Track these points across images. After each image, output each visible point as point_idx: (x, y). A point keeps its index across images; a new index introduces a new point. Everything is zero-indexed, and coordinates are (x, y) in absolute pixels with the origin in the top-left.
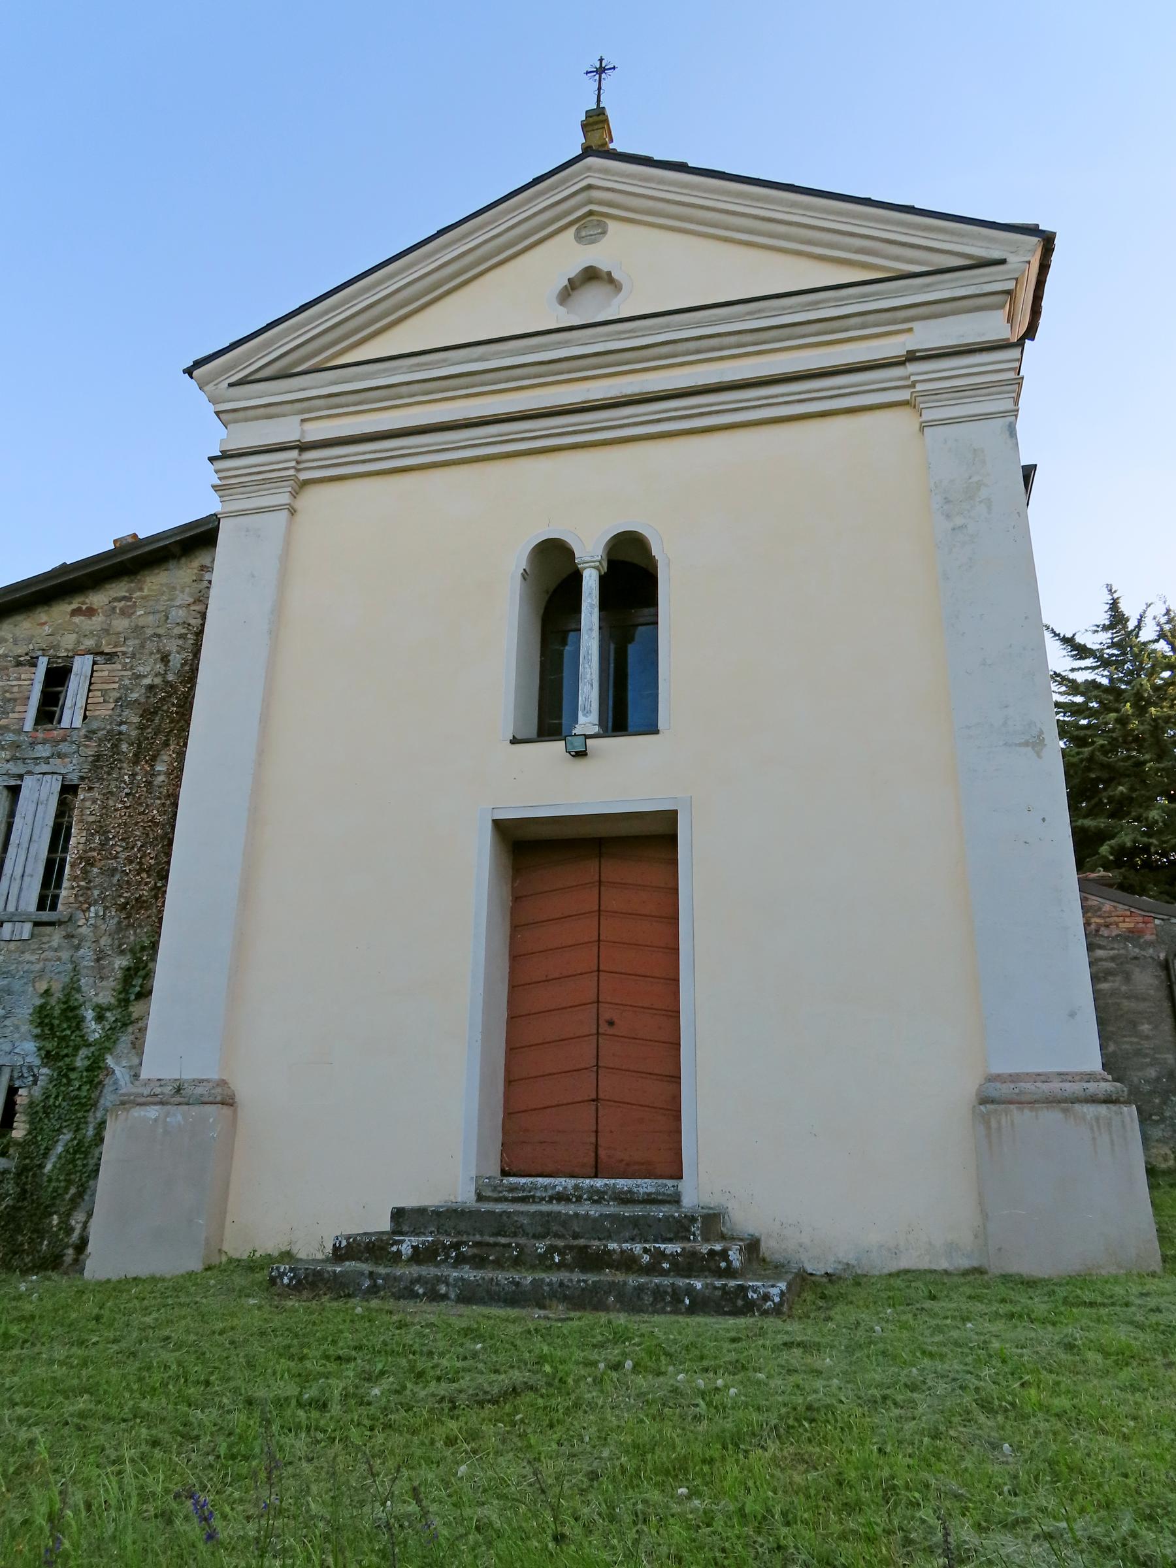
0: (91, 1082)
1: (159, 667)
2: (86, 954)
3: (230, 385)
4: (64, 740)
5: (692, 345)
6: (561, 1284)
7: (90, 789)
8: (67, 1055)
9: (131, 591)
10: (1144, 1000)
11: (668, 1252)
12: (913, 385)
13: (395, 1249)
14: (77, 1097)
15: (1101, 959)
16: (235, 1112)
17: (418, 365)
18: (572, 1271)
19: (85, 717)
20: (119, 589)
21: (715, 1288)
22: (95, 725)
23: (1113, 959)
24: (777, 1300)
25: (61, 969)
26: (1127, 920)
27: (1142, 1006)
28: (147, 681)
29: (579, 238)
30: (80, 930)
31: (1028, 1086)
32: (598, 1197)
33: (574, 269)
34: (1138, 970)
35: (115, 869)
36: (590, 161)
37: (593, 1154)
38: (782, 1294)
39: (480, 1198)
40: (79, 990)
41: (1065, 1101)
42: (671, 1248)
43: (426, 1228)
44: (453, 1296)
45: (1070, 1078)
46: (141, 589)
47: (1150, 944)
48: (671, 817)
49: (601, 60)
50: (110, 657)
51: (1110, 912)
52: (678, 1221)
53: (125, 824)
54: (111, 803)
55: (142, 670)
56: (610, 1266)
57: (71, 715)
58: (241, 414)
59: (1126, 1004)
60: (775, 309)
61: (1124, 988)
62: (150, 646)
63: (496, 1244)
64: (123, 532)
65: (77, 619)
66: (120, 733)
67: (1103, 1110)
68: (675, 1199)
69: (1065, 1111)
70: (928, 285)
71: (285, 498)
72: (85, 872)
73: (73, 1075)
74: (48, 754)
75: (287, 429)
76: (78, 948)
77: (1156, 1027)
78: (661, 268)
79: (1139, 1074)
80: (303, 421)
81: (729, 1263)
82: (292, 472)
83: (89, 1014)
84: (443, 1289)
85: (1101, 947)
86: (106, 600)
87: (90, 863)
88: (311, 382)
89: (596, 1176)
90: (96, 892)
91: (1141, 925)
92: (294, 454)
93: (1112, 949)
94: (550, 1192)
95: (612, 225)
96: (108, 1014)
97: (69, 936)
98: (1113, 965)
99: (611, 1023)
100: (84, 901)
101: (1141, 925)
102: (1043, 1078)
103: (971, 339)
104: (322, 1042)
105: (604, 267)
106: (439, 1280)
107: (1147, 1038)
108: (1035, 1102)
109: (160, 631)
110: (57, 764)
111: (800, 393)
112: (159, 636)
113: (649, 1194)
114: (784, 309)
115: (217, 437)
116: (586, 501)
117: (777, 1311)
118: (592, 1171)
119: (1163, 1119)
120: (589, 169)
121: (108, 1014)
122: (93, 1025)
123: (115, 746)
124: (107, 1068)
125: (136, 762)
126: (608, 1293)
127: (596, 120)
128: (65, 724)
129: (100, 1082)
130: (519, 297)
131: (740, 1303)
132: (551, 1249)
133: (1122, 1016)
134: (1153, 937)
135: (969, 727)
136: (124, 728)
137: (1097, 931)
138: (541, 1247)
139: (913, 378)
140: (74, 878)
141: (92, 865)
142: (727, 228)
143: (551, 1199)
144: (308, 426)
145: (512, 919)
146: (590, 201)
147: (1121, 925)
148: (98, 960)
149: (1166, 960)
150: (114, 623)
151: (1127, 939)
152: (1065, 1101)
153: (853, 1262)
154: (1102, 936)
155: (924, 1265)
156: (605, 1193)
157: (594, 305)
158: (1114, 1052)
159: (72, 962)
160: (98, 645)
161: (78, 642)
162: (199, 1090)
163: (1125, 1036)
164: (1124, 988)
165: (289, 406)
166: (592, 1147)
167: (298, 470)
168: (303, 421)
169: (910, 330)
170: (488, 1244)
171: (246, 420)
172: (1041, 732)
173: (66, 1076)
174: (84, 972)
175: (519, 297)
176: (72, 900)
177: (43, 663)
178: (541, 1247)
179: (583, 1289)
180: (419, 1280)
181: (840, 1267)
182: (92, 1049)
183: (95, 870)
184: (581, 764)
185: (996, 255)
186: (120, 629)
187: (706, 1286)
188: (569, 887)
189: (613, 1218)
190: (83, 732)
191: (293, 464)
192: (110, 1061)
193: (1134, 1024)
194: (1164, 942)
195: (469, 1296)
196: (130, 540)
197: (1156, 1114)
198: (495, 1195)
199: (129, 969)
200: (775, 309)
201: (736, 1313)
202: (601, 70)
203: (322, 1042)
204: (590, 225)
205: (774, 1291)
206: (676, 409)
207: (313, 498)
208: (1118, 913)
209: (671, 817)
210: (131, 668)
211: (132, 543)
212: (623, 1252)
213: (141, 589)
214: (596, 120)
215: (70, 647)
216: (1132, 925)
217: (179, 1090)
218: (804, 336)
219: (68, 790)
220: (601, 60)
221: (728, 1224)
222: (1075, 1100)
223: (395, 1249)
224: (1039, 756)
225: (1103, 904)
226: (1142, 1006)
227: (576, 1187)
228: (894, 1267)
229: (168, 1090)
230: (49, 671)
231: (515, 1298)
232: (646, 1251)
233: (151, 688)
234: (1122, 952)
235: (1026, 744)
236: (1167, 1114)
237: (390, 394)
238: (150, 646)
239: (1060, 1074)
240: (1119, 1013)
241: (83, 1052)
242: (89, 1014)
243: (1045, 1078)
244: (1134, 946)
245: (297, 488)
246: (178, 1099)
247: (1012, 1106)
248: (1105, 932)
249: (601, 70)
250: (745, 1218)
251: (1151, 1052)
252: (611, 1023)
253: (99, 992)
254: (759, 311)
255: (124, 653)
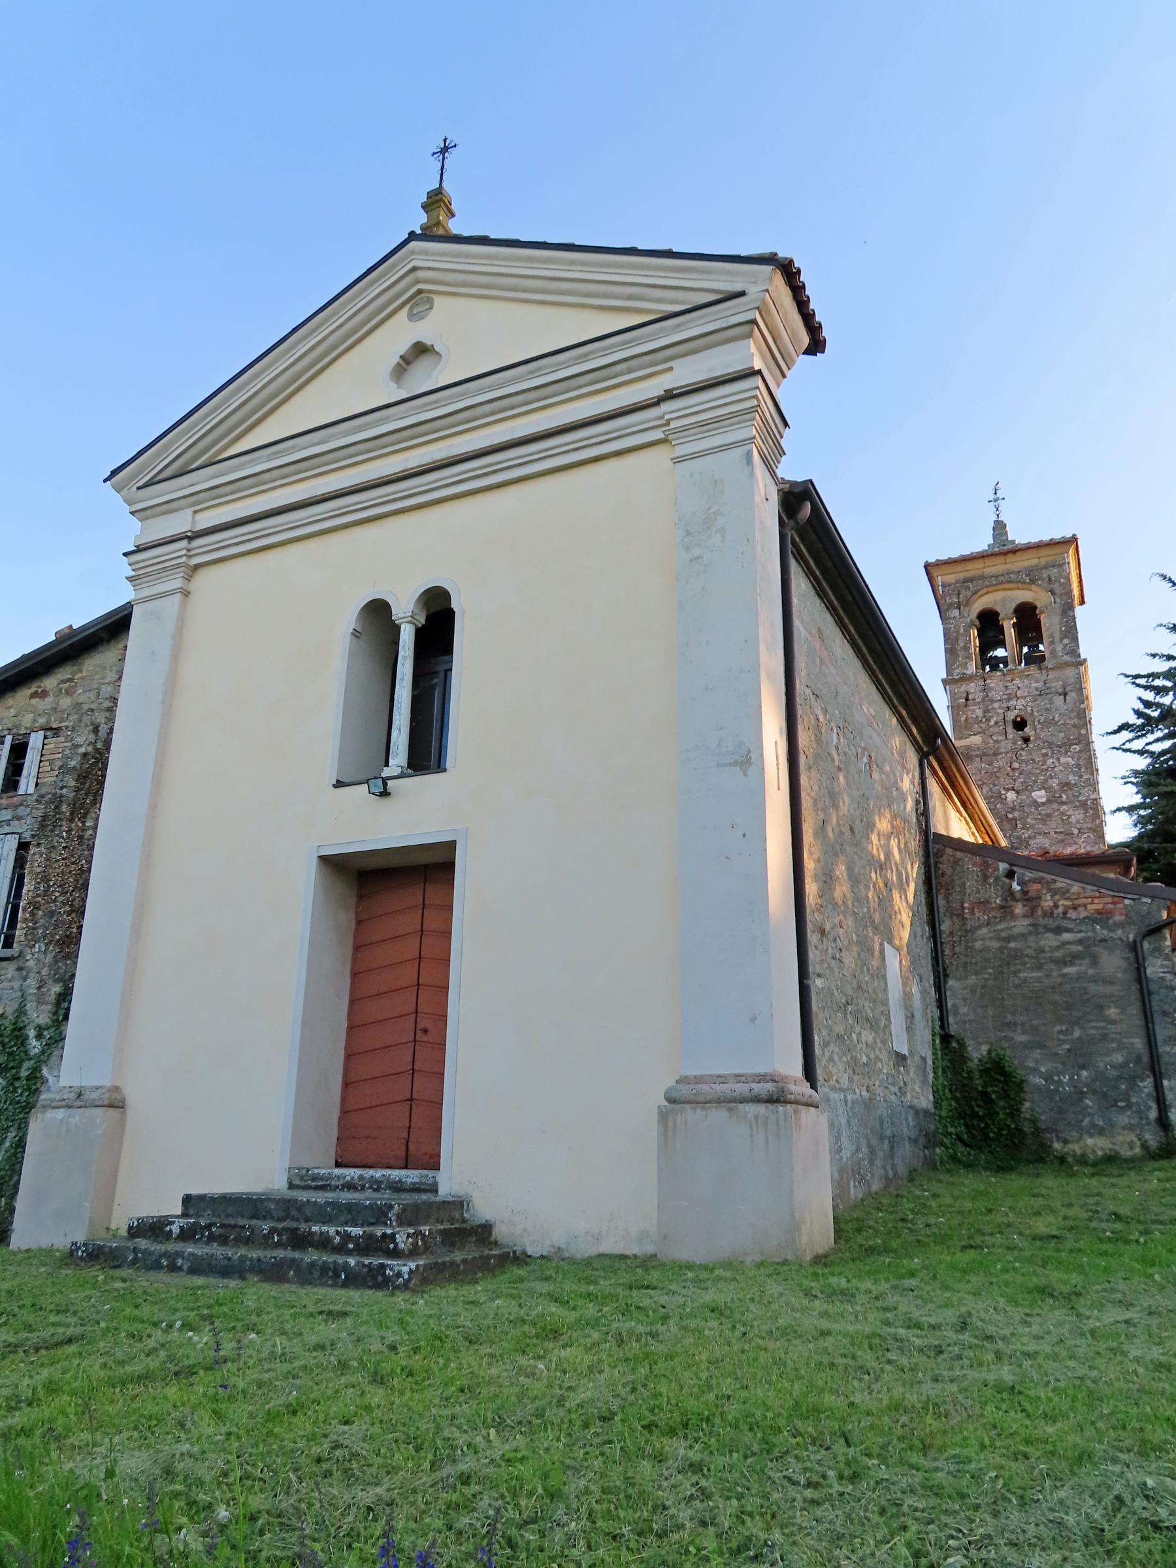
0: (29, 1089)
1: (92, 737)
2: (32, 983)
3: (138, 488)
4: (21, 805)
5: (487, 408)
6: (259, 1260)
7: (39, 845)
8: (13, 1068)
9: (74, 674)
10: (1112, 983)
11: (353, 1234)
12: (668, 423)
13: (168, 1228)
14: (19, 1102)
15: (1069, 943)
16: (123, 1114)
17: (275, 453)
18: (286, 1249)
19: (37, 784)
20: (64, 673)
21: (364, 1266)
22: (44, 790)
23: (1080, 942)
24: (406, 1277)
25: (14, 996)
26: (1096, 901)
27: (1109, 989)
28: (82, 750)
29: (411, 317)
30: (28, 963)
31: (705, 1087)
32: (376, 1185)
33: (404, 346)
34: (1106, 952)
35: (54, 911)
36: (413, 245)
37: (404, 1148)
38: (411, 1272)
39: (291, 1186)
40: (25, 1013)
41: (734, 1100)
42: (356, 1231)
43: (205, 1211)
44: (185, 1268)
45: (744, 1079)
46: (81, 671)
47: (1118, 925)
48: (450, 847)
49: (445, 140)
50: (56, 731)
51: (1078, 894)
52: (380, 1208)
53: (62, 872)
54: (53, 855)
55: (79, 740)
56: (312, 1245)
57: (27, 784)
58: (149, 512)
59: (1093, 988)
60: (551, 366)
61: (1091, 972)
62: (86, 719)
63: (235, 1226)
64: (62, 625)
65: (34, 701)
66: (61, 796)
67: (762, 1109)
68: (433, 1189)
69: (730, 1110)
70: (680, 325)
71: (178, 583)
72: (33, 914)
73: (17, 1084)
74: (9, 817)
75: (180, 522)
76: (25, 979)
77: (1123, 1011)
78: (476, 334)
79: (1107, 1059)
80: (195, 512)
81: (396, 1244)
82: (184, 559)
83: (32, 1033)
84: (180, 1262)
85: (1068, 930)
86: (56, 682)
87: (37, 907)
88: (202, 478)
89: (406, 1168)
90: (40, 931)
91: (1110, 906)
92: (184, 543)
93: (1081, 931)
94: (342, 1182)
95: (437, 300)
96: (45, 1033)
97: (20, 969)
98: (1080, 948)
99: (425, 1031)
100: (32, 941)
101: (1110, 906)
102: (721, 1080)
103: (720, 372)
104: (194, 1053)
105: (428, 342)
106: (179, 1254)
107: (1114, 1022)
108: (710, 1102)
109: (93, 706)
110: (17, 826)
111: (573, 443)
112: (92, 710)
113: (415, 1184)
114: (559, 364)
115: (132, 531)
116: (397, 562)
117: (406, 1286)
118: (402, 1163)
119: (1129, 1106)
120: (412, 252)
121: (45, 1033)
122: (34, 1042)
123: (57, 807)
124: (42, 1077)
125: (71, 820)
126: (290, 1267)
127: (436, 201)
128: (21, 791)
129: (37, 1089)
130: (361, 379)
131: (380, 1278)
132: (273, 1230)
133: (1088, 1000)
134: (1123, 918)
135: (687, 750)
136: (64, 791)
137: (1065, 913)
138: (266, 1227)
139: (667, 417)
140: (25, 920)
141: (38, 909)
142: (524, 291)
143: (343, 1186)
144: (200, 516)
145: (355, 937)
146: (418, 282)
147: (1089, 907)
148: (39, 988)
149: (1135, 941)
150: (61, 702)
151: (1095, 921)
152: (734, 1100)
153: (563, 1246)
154: (1070, 919)
155: (618, 1250)
156: (381, 1182)
157: (425, 377)
158: (1080, 1038)
159: (21, 990)
160: (48, 723)
161: (34, 721)
162: (94, 1096)
163: (1091, 1021)
164: (1091, 972)
165: (183, 501)
166: (404, 1142)
167: (190, 557)
168: (195, 512)
169: (671, 369)
170: (230, 1226)
171: (154, 516)
172: (749, 752)
173: (12, 1084)
174: (29, 998)
175: (361, 379)
176: (23, 938)
177: (8, 740)
178: (266, 1227)
179: (273, 1264)
180: (165, 1255)
181: (553, 1250)
182: (32, 1062)
183: (41, 913)
184: (386, 802)
185: (738, 287)
186: (65, 707)
187: (357, 1263)
188: (399, 909)
189: (334, 1204)
190: (35, 797)
191: (184, 552)
192: (45, 1072)
193: (1101, 1008)
194: (1134, 923)
195: (198, 1267)
196: (67, 631)
197: (1121, 1100)
198: (303, 1184)
199: (60, 994)
200: (551, 366)
201: (377, 1286)
202: (445, 150)
203: (194, 1053)
204: (418, 301)
205: (405, 1269)
206: (473, 470)
207: (204, 579)
208: (1087, 894)
209: (450, 847)
210: (71, 740)
211: (68, 634)
212: (321, 1233)
213: (81, 671)
214: (436, 201)
215: (28, 725)
216: (1100, 907)
217: (80, 1095)
218: (580, 387)
219: (23, 846)
220: (445, 140)
221: (471, 1211)
222: (743, 1100)
223: (168, 1228)
224: (745, 775)
225: (1072, 886)
226: (1109, 989)
227: (361, 1177)
228: (594, 1251)
229: (72, 1096)
230: (12, 746)
231: (226, 1271)
232: (338, 1233)
233: (85, 755)
234: (1090, 934)
235: (735, 763)
236: (1134, 1100)
237: (256, 482)
238: (86, 719)
239: (737, 1076)
240: (1086, 997)
241: (27, 1064)
242: (32, 1033)
243: (722, 1079)
244: (1102, 928)
245: (190, 573)
246: (78, 1103)
247: (687, 1106)
248: (1072, 915)
249: (445, 150)
250: (483, 1209)
251: (1118, 1037)
252: (425, 1031)
253: (39, 1015)
254: (539, 369)
255: (67, 727)
